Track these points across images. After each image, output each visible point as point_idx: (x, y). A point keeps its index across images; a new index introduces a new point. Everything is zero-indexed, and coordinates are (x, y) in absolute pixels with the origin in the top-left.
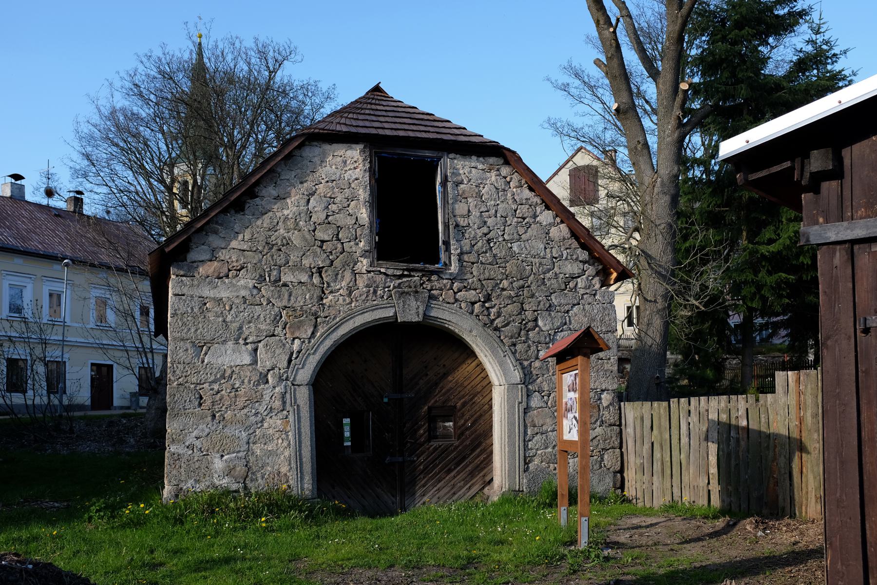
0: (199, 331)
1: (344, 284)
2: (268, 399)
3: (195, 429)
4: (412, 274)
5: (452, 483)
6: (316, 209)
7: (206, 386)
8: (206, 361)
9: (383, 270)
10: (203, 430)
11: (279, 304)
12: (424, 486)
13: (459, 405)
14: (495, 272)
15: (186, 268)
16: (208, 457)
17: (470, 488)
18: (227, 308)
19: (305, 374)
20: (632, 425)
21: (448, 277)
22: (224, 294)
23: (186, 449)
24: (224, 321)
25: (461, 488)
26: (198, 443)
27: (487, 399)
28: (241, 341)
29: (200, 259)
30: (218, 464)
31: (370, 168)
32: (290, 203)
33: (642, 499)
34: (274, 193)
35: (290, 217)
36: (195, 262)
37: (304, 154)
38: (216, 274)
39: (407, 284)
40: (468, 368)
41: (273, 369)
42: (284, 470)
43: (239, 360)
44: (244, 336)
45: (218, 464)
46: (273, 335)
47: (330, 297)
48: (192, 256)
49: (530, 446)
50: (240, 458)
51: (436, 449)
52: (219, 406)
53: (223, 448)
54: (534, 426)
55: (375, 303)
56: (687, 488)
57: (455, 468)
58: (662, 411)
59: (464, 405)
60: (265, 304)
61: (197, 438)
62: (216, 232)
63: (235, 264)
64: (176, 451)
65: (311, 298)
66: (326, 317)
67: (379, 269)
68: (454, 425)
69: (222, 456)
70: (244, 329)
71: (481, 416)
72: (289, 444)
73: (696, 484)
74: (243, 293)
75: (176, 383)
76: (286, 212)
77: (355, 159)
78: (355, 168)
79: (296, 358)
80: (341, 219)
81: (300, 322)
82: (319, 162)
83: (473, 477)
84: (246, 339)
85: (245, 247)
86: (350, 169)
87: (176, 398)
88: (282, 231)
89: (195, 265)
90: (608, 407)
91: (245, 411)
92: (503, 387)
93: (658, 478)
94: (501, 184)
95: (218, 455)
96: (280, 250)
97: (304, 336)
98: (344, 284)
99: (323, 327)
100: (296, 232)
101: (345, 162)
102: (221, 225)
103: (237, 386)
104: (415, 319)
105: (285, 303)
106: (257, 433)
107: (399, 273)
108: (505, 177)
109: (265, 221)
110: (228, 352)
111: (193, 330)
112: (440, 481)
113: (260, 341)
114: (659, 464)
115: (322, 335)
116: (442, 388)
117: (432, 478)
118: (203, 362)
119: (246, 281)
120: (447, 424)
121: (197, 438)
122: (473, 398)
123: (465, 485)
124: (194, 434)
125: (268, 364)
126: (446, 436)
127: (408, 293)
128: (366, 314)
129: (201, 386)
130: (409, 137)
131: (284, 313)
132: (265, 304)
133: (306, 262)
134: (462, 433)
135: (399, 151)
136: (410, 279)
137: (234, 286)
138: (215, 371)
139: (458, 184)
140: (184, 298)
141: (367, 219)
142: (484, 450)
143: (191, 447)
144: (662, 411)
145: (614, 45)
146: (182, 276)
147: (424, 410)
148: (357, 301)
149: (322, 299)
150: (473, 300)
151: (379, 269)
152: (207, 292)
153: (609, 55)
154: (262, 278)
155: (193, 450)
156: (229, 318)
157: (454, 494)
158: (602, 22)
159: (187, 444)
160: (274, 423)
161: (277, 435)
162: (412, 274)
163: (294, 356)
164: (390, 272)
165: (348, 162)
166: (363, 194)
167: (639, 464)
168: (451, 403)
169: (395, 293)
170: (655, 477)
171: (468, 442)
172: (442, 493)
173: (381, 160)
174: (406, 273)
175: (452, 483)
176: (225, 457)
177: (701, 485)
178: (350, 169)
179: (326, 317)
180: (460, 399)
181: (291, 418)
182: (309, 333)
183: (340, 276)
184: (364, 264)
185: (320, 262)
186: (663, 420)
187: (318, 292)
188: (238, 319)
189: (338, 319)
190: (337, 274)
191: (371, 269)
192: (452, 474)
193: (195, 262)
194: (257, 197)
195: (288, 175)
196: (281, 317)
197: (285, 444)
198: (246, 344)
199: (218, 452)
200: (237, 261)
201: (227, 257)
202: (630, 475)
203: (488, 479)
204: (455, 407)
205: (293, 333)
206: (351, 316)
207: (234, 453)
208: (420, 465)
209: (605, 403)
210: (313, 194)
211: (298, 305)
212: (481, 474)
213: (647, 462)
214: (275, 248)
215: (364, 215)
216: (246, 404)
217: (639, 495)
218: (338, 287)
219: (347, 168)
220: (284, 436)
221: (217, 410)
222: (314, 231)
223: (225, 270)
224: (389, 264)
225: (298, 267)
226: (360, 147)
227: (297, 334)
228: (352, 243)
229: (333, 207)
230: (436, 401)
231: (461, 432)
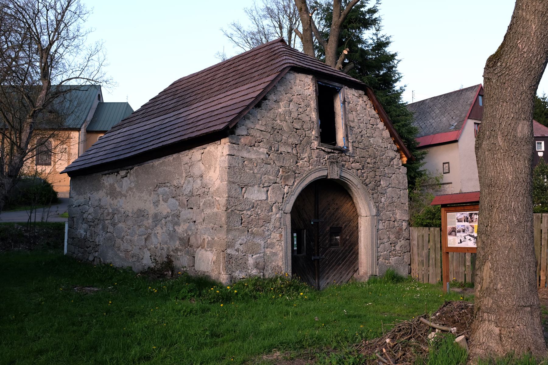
0: (242, 178)
1: (306, 155)
2: (273, 221)
3: (240, 239)
4: (335, 151)
5: (340, 271)
6: (293, 110)
7: (244, 212)
8: (245, 197)
9: (323, 148)
10: (243, 240)
11: (278, 164)
12: (328, 273)
13: (343, 226)
14: (365, 153)
15: (235, 139)
16: (246, 256)
17: (348, 274)
18: (255, 165)
19: (289, 207)
20: (416, 239)
21: (348, 155)
22: (253, 156)
23: (235, 252)
24: (253, 173)
25: (345, 274)
26: (241, 248)
27: (356, 224)
28: (261, 185)
29: (242, 134)
30: (251, 261)
31: (315, 89)
32: (281, 105)
33: (422, 280)
34: (275, 98)
35: (282, 113)
36: (239, 135)
37: (287, 78)
38: (250, 144)
39: (332, 157)
40: (347, 206)
41: (275, 203)
42: (280, 264)
43: (260, 197)
44: (263, 182)
45: (251, 261)
46: (276, 183)
47: (301, 162)
48: (239, 131)
49: (379, 251)
50: (261, 257)
51: (333, 252)
52: (251, 225)
53: (253, 251)
54: (380, 239)
55: (320, 167)
56: (452, 273)
57: (342, 262)
58: (436, 232)
59: (346, 226)
60: (272, 164)
61: (241, 244)
62: (249, 119)
63: (258, 139)
64: (230, 253)
65: (293, 162)
66: (299, 174)
67: (321, 148)
68: (341, 238)
69: (252, 256)
70: (263, 178)
71: (353, 233)
72: (282, 249)
73: (457, 271)
74: (262, 156)
75: (230, 210)
76: (280, 110)
77: (309, 84)
78: (309, 89)
79: (286, 197)
80: (303, 117)
81: (288, 175)
82: (293, 83)
83: (349, 268)
84: (263, 184)
85: (263, 129)
86: (307, 89)
87: (230, 220)
88: (279, 121)
89: (240, 137)
90: (405, 230)
91: (263, 228)
92: (368, 217)
93: (433, 268)
94: (364, 105)
95: (251, 255)
96: (278, 132)
97: (290, 184)
98: (306, 155)
99: (298, 179)
100: (285, 122)
101: (304, 84)
102: (251, 114)
103: (259, 212)
104: (337, 178)
105: (281, 164)
106: (268, 242)
107: (330, 150)
108: (365, 102)
109: (271, 114)
110: (256, 192)
111: (239, 177)
112: (335, 270)
113: (270, 186)
114: (434, 260)
115: (297, 184)
116: (336, 216)
117: (331, 269)
118: (243, 197)
119: (263, 150)
120: (337, 237)
121: (241, 244)
122: (349, 223)
123: (346, 272)
124: (239, 242)
125: (274, 200)
126: (336, 244)
127: (334, 162)
128: (316, 173)
129: (242, 212)
130: (333, 75)
131: (281, 170)
132: (272, 164)
133: (290, 141)
134: (345, 243)
135: (326, 81)
136: (333, 154)
137: (258, 152)
138: (249, 203)
139: (349, 103)
140: (234, 157)
141: (315, 119)
142: (354, 252)
143: (237, 250)
144: (436, 232)
145: (309, 23)
146: (233, 143)
147: (328, 229)
148: (312, 165)
149: (297, 163)
150: (358, 168)
151: (321, 148)
152: (245, 155)
153: (306, 28)
154: (271, 148)
155: (238, 252)
156: (256, 171)
157: (341, 278)
158: (303, 10)
159: (236, 248)
160: (275, 235)
161: (277, 243)
162: (335, 151)
163: (285, 195)
164: (326, 150)
165: (306, 85)
166: (313, 104)
167: (421, 261)
168: (339, 226)
169: (329, 162)
170: (431, 268)
171: (347, 248)
172: (335, 277)
173: (319, 85)
174: (332, 151)
175: (340, 271)
176: (254, 257)
177: (461, 271)
178: (307, 89)
179: (299, 174)
180: (344, 223)
181: (283, 233)
182: (292, 182)
183: (305, 150)
184: (315, 144)
185: (296, 141)
186: (436, 237)
187: (296, 159)
188: (260, 172)
189: (304, 175)
190: (304, 149)
191: (318, 147)
192: (340, 266)
193: (239, 135)
194: (267, 99)
195: (281, 89)
196: (279, 172)
197: (280, 248)
198: (264, 187)
199: (251, 253)
200: (259, 137)
201: (255, 134)
202: (415, 266)
203: (356, 269)
204: (342, 227)
205: (285, 182)
206: (310, 173)
207: (258, 254)
208: (326, 261)
209: (404, 228)
210: (291, 101)
211: (287, 165)
212: (353, 266)
213: (426, 260)
214: (276, 131)
215: (314, 116)
216: (263, 224)
217: (421, 277)
218: (304, 156)
219: (305, 88)
220: (280, 244)
221: (250, 227)
222: (292, 123)
223: (253, 142)
224: (326, 145)
225: (286, 144)
226: (311, 77)
227: (287, 183)
228: (309, 132)
229: (300, 110)
230: (333, 224)
231: (344, 241)
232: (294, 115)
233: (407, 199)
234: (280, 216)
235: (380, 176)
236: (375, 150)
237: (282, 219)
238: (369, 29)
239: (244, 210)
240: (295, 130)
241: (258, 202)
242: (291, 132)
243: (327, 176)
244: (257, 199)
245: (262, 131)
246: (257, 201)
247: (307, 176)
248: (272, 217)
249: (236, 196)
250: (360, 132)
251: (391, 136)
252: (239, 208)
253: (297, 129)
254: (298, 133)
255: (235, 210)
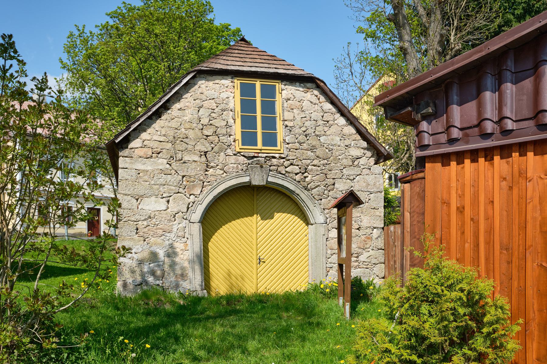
7: (140, 222)
16: (142, 265)
29: (136, 147)
79: (192, 206)
88: (183, 130)
90: (377, 238)
110: (153, 203)
113: (171, 196)
129: (137, 223)
152: (140, 167)
232: (205, 121)
233: (382, 204)
234: (184, 226)
235: (333, 179)
236: (327, 150)
237: (187, 228)
238: (112, 16)
239: (139, 221)
240: (205, 137)
241: (156, 212)
242: (198, 140)
243: (250, 182)
244: (155, 209)
245: (161, 142)
246: (155, 211)
247: (219, 184)
248: (173, 227)
249: (129, 207)
250: (304, 132)
251: (357, 132)
252: (133, 219)
253: (207, 136)
254: (208, 140)
255: (129, 220)
